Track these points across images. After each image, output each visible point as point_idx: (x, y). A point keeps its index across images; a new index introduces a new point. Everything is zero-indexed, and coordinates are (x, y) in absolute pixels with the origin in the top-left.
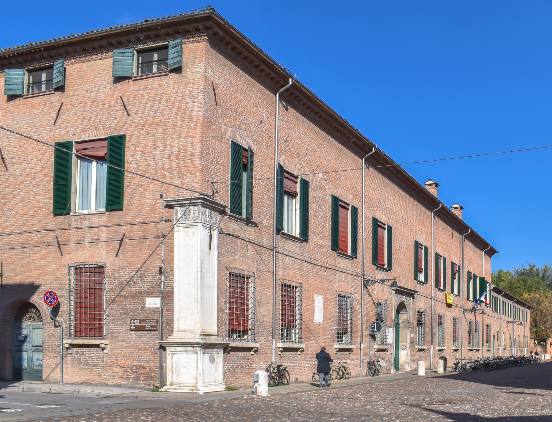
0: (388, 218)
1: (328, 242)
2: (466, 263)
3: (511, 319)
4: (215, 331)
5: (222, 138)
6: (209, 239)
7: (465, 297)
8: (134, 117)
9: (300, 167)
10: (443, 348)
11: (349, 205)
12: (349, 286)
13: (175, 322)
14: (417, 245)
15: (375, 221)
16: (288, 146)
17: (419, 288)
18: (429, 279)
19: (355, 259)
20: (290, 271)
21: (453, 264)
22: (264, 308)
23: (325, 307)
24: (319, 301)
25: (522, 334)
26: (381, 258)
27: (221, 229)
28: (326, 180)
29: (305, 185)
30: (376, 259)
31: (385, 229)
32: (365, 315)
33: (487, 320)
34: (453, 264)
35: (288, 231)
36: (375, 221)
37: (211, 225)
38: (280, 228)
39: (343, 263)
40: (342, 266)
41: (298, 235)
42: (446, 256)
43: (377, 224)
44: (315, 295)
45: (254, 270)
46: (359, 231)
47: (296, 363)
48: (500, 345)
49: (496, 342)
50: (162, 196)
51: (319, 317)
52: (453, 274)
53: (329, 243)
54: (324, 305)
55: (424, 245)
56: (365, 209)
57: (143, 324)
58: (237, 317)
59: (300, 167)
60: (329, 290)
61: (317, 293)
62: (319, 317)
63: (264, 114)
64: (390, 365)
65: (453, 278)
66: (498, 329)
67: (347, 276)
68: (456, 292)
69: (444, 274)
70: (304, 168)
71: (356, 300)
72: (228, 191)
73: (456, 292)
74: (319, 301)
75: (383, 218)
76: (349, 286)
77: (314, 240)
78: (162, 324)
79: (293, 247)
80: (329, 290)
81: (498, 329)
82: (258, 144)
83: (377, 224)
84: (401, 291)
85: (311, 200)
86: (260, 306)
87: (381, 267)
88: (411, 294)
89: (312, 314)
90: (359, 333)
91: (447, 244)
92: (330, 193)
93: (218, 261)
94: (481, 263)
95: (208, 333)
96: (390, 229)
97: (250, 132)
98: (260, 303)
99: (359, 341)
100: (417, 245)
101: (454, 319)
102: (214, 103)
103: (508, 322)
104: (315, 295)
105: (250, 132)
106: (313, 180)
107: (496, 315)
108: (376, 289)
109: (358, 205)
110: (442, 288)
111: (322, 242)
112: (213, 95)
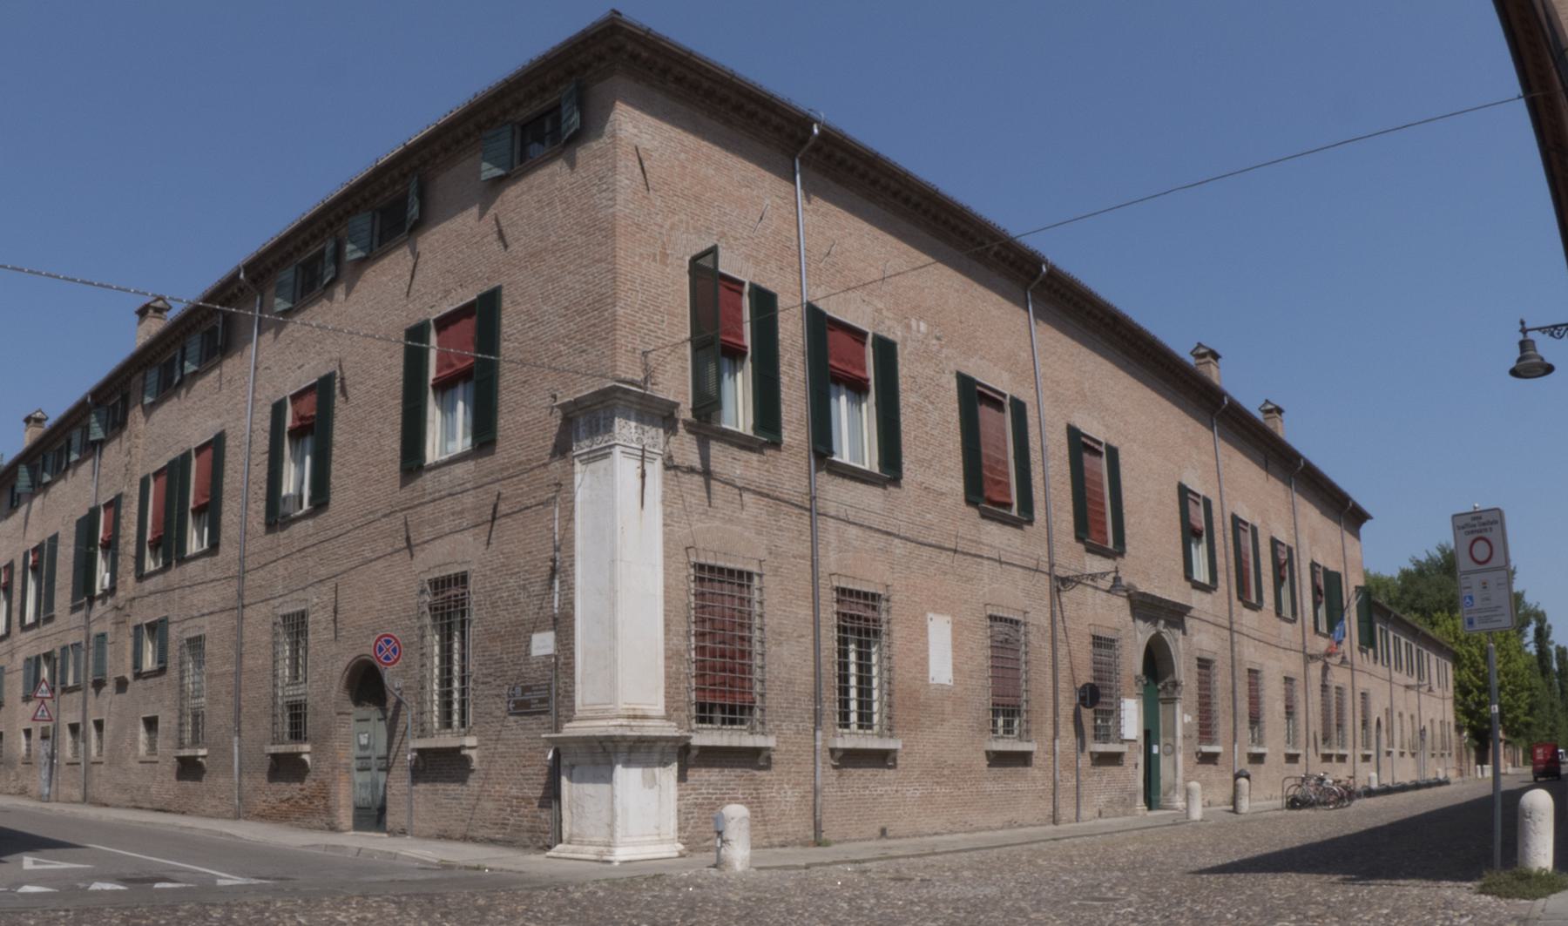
0: (1107, 427)
1: (955, 484)
2: (1304, 541)
3: (1413, 681)
4: (659, 707)
5: (665, 255)
6: (639, 482)
7: (1309, 623)
8: (514, 247)
9: (869, 309)
10: (1261, 750)
11: (1004, 395)
12: (1021, 595)
13: (578, 687)
14: (1184, 492)
15: (1074, 434)
16: (833, 265)
17: (1196, 600)
18: (1221, 576)
19: (1027, 527)
20: (855, 559)
21: (1274, 543)
22: (790, 645)
23: (957, 646)
24: (939, 632)
25: (1438, 718)
26: (1100, 521)
27: (670, 458)
28: (938, 339)
29: (886, 351)
30: (1085, 527)
31: (1099, 454)
32: (1063, 665)
33: (1363, 683)
34: (1274, 543)
35: (853, 456)
36: (1074, 434)
37: (643, 450)
38: (823, 449)
39: (996, 536)
40: (997, 543)
41: (876, 470)
42: (1257, 522)
43: (1079, 444)
44: (930, 615)
45: (763, 554)
46: (1035, 456)
47: (881, 790)
48: (1391, 743)
49: (1383, 735)
50: (554, 397)
51: (941, 668)
52: (1278, 567)
53: (958, 486)
54: (954, 639)
55: (1202, 492)
56: (1046, 406)
57: (528, 696)
58: (720, 675)
59: (869, 309)
60: (966, 602)
61: (935, 611)
62: (941, 668)
63: (768, 202)
64: (1133, 795)
65: (1278, 581)
66: (1387, 704)
67: (1010, 567)
68: (1287, 611)
69: (1257, 572)
70: (879, 311)
71: (1038, 627)
72: (684, 369)
73: (1287, 611)
74: (939, 632)
75: (1092, 428)
76: (1021, 595)
77: (920, 478)
78: (558, 695)
79: (869, 498)
80: (966, 602)
81: (1387, 704)
82: (757, 264)
83: (1079, 444)
84: (1145, 607)
85: (903, 384)
86: (780, 644)
87: (1097, 550)
88: (1176, 614)
89: (923, 663)
90: (1050, 714)
91: (1249, 493)
92: (953, 367)
93: (665, 533)
94: (1339, 542)
95: (639, 713)
96: (1113, 453)
97: (736, 239)
98: (780, 634)
99: (1050, 732)
100: (1184, 492)
101: (1288, 680)
102: (642, 188)
103: (1408, 687)
104: (930, 615)
105: (736, 239)
106: (905, 339)
107: (1380, 669)
108: (1090, 601)
109: (1026, 395)
110: (1254, 600)
111: (941, 484)
112: (638, 170)
